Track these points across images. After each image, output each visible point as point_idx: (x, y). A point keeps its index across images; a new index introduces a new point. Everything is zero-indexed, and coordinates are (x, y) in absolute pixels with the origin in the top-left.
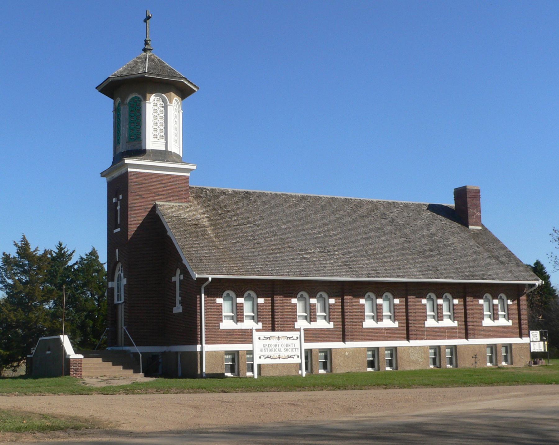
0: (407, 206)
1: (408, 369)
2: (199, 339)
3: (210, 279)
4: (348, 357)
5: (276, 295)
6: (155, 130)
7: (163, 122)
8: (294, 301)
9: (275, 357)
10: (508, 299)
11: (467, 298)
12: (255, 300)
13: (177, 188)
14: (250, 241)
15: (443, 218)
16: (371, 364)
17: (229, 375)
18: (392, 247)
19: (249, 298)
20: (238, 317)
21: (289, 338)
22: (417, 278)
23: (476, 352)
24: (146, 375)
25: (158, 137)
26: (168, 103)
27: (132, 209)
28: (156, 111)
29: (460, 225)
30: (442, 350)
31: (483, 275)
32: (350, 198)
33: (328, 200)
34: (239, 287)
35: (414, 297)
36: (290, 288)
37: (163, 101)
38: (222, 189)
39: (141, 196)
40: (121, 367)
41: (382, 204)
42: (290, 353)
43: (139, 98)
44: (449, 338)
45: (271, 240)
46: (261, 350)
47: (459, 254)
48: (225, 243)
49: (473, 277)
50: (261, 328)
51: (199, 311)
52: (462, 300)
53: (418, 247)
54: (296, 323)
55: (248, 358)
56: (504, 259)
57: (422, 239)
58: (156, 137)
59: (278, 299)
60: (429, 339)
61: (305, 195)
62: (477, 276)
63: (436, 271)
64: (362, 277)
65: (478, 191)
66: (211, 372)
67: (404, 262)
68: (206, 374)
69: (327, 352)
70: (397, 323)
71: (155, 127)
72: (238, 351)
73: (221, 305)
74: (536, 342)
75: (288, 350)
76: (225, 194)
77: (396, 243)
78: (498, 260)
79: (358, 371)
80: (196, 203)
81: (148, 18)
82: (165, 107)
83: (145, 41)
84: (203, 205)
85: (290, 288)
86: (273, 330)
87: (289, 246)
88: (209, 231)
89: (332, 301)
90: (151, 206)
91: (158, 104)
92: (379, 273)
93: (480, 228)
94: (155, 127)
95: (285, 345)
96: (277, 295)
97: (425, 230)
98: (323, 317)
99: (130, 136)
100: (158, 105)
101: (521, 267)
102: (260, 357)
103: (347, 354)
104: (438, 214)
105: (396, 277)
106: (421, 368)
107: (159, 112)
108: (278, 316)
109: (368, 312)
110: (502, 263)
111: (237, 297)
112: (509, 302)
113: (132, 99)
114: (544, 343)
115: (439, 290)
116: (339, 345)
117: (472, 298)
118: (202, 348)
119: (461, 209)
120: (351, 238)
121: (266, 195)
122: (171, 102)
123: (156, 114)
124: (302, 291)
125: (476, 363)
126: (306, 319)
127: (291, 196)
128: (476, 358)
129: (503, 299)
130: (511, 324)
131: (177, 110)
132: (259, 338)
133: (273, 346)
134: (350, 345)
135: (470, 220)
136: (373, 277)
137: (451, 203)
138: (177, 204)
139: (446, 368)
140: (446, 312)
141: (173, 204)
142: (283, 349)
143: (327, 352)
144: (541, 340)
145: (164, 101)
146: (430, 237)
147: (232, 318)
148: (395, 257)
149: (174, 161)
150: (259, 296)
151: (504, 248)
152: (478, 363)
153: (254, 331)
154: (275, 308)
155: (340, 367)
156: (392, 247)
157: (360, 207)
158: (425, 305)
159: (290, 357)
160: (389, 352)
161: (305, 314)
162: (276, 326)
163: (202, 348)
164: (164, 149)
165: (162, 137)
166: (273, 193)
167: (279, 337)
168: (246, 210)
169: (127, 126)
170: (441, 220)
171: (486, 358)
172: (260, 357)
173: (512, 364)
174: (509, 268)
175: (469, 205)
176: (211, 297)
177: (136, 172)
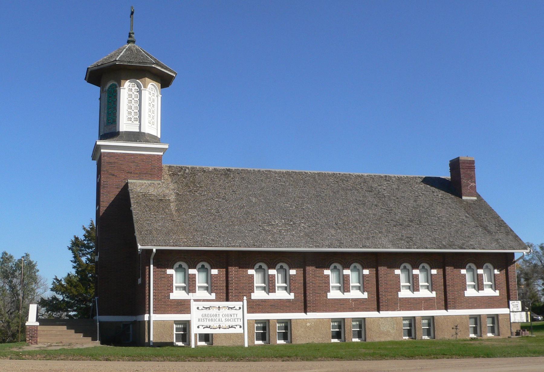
0: (399, 179)
1: (377, 340)
3: (154, 250)
4: (310, 328)
5: (229, 266)
6: (130, 113)
7: (137, 105)
8: (397, 272)
9: (215, 326)
10: (495, 268)
11: (447, 267)
12: (475, 271)
13: (150, 167)
14: (212, 214)
15: (437, 190)
16: (337, 335)
17: (180, 344)
18: (368, 218)
19: (355, 269)
21: (231, 308)
22: (385, 248)
23: (456, 324)
25: (133, 120)
26: (143, 88)
27: (104, 187)
28: (130, 96)
29: (453, 197)
30: (417, 321)
31: (463, 244)
32: (338, 173)
33: (313, 176)
34: (192, 258)
35: (385, 268)
36: (246, 259)
37: (138, 87)
38: (204, 167)
39: (113, 175)
40: (82, 335)
41: (372, 178)
42: (233, 323)
43: (116, 85)
45: (235, 213)
46: (199, 320)
47: (443, 224)
48: (184, 216)
49: (451, 247)
50: (214, 298)
51: (147, 282)
52: (441, 271)
53: (397, 218)
55: (353, 325)
56: (492, 228)
57: (406, 210)
58: (130, 119)
59: (233, 270)
60: (403, 310)
61: (290, 171)
62: (455, 245)
63: (410, 241)
64: (322, 247)
65: (473, 162)
66: (159, 341)
67: (376, 233)
68: (153, 343)
69: (430, 319)
70: (366, 293)
71: (130, 110)
73: (172, 276)
74: (516, 313)
75: (229, 320)
76: (204, 171)
77: (374, 215)
78: (486, 230)
79: (321, 342)
80: (170, 180)
81: (132, 13)
82: (140, 92)
83: (130, 33)
84: (176, 182)
85: (246, 259)
86: (227, 300)
87: (252, 219)
88: (173, 206)
89: (293, 272)
90: (123, 184)
91: (133, 89)
92: (343, 243)
93: (475, 198)
94: (130, 110)
96: (231, 266)
97: (412, 202)
98: (284, 288)
99: (108, 120)
101: (510, 236)
102: (198, 327)
103: (308, 324)
104: (432, 186)
105: (361, 248)
106: (392, 339)
107: (133, 97)
108: (232, 286)
109: (469, 282)
110: (489, 232)
111: (189, 268)
112: (496, 272)
113: (110, 86)
114: (527, 314)
116: (301, 316)
118: (150, 317)
119: (455, 182)
120: (325, 210)
121: (248, 172)
122: (145, 87)
123: (130, 99)
124: (356, 262)
125: (456, 334)
126: (286, 290)
127: (275, 173)
128: (457, 329)
130: (498, 295)
131: (156, 95)
132: (198, 308)
133: (213, 315)
134: (311, 315)
135: (463, 191)
136: (334, 247)
137: (446, 175)
138: (149, 182)
139: (422, 339)
140: (486, 282)
141: (145, 181)
142: (223, 319)
143: (287, 323)
144: (523, 310)
145: (139, 86)
146: (415, 208)
147: (339, 288)
148: (367, 228)
149: (147, 141)
150: (432, 268)
151: (497, 218)
152: (459, 334)
153: (192, 301)
154: (230, 279)
155: (300, 338)
156: (368, 218)
157: (347, 181)
158: (398, 276)
159: (232, 327)
160: (358, 323)
161: (427, 284)
162: (230, 297)
163: (150, 317)
164: (138, 131)
165: (136, 120)
166: (256, 169)
167: (219, 307)
168: (220, 186)
169: (106, 111)
170: (433, 192)
171: (468, 329)
172: (198, 327)
173: (499, 335)
174: (496, 237)
175: (462, 176)
176: (242, 268)
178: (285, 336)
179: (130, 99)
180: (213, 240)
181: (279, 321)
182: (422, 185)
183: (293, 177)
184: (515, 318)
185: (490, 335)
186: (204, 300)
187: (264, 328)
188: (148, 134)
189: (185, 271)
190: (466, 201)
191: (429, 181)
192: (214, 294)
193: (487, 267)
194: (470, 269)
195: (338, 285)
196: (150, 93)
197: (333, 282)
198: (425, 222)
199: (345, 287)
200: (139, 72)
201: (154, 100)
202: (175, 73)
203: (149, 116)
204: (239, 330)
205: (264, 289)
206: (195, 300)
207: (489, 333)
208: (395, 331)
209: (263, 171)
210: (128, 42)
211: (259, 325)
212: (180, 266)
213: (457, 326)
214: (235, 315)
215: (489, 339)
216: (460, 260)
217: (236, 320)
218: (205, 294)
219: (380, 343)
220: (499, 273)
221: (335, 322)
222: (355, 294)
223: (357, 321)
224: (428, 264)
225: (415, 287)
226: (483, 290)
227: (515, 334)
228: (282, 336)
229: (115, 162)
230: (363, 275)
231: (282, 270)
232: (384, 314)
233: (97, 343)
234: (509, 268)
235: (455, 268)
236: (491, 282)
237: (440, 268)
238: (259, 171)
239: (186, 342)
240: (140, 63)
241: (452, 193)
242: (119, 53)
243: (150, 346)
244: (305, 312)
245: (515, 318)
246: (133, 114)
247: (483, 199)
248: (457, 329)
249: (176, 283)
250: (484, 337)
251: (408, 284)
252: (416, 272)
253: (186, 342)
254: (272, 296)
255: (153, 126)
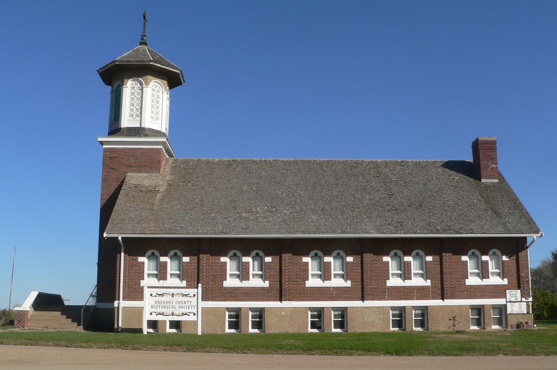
2: (117, 295)
5: (200, 253)
6: (132, 110)
9: (168, 313)
10: (503, 255)
11: (444, 254)
13: (148, 161)
20: (406, 274)
22: (367, 233)
23: (454, 315)
24: (86, 328)
25: (134, 116)
28: (133, 93)
29: (472, 180)
30: (407, 311)
31: (461, 229)
33: (321, 164)
35: (372, 255)
37: (140, 84)
40: (70, 320)
44: (418, 299)
46: (152, 307)
49: (445, 231)
50: (185, 286)
52: (438, 258)
54: (466, 280)
59: (204, 257)
60: (392, 299)
65: (494, 143)
66: (128, 327)
69: (402, 310)
72: (427, 307)
73: (387, 263)
75: (182, 307)
82: (142, 90)
91: (136, 87)
93: (497, 181)
95: (179, 302)
96: (203, 253)
100: (136, 89)
101: (523, 220)
102: (151, 314)
103: (283, 313)
107: (136, 94)
111: (184, 256)
112: (505, 258)
115: (407, 246)
117: (451, 254)
118: (119, 304)
123: (133, 96)
125: (454, 325)
126: (401, 277)
127: (282, 162)
128: (454, 320)
129: (477, 256)
131: (161, 91)
132: (151, 295)
134: (286, 304)
135: (483, 173)
142: (177, 306)
145: (141, 84)
147: (478, 275)
149: (146, 136)
154: (201, 267)
155: (273, 326)
159: (185, 314)
163: (119, 304)
167: (173, 294)
171: (469, 320)
172: (151, 314)
176: (215, 255)
177: (110, 148)
178: (422, 323)
179: (133, 96)
180: (182, 227)
181: (415, 308)
182: (440, 170)
183: (298, 166)
184: (512, 309)
185: (496, 327)
186: (174, 288)
187: (423, 315)
188: (149, 129)
189: (157, 259)
190: (485, 184)
191: (451, 165)
192: (185, 281)
193: (494, 253)
194: (473, 256)
195: (319, 272)
196: (153, 90)
197: (471, 268)
198: (426, 206)
199: (325, 275)
200: (140, 70)
201: (158, 97)
202: (178, 70)
203: (152, 112)
204: (192, 318)
205: (400, 276)
206: (149, 287)
207: (495, 324)
208: (381, 321)
209: (270, 161)
210: (141, 44)
211: (337, 313)
212: (153, 254)
213: (454, 317)
214: (189, 303)
215: (474, 333)
216: (459, 246)
217: (190, 307)
218: (176, 282)
219: (364, 334)
220: (508, 259)
221: (314, 311)
222: (337, 282)
223: (339, 311)
224: (422, 250)
225: (484, 274)
226: (489, 278)
227: (515, 326)
228: (420, 323)
229: (115, 157)
230: (348, 263)
231: (258, 257)
232: (368, 303)
233: (80, 329)
234: (520, 254)
235: (453, 255)
236: (499, 269)
237: (437, 255)
238: (265, 161)
239: (480, 325)
240: (138, 61)
241: (471, 176)
242: (124, 55)
243: (119, 332)
244: (443, 299)
245: (512, 309)
246: (135, 111)
247: (506, 181)
248: (454, 320)
249: (312, 271)
250: (488, 329)
251: (399, 272)
252: (485, 258)
253: (480, 325)
254: (245, 284)
255: (156, 121)
